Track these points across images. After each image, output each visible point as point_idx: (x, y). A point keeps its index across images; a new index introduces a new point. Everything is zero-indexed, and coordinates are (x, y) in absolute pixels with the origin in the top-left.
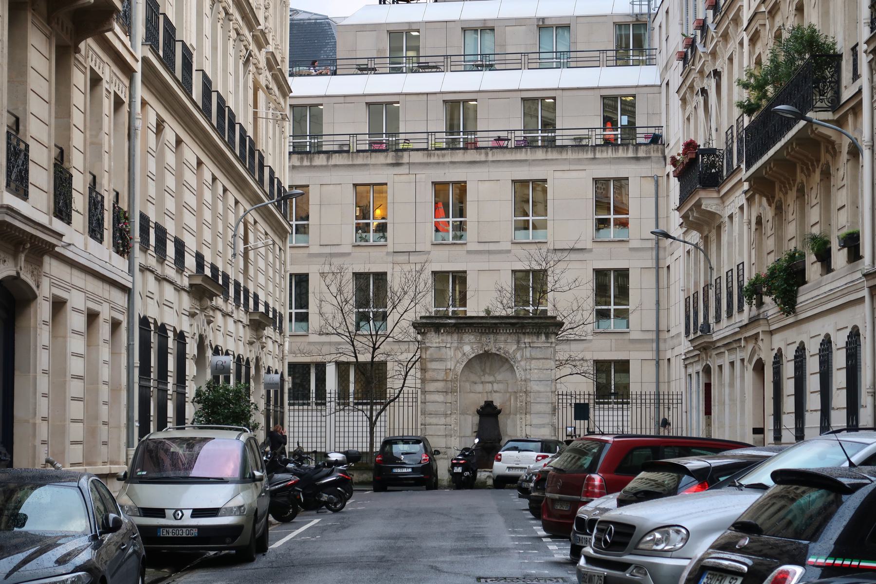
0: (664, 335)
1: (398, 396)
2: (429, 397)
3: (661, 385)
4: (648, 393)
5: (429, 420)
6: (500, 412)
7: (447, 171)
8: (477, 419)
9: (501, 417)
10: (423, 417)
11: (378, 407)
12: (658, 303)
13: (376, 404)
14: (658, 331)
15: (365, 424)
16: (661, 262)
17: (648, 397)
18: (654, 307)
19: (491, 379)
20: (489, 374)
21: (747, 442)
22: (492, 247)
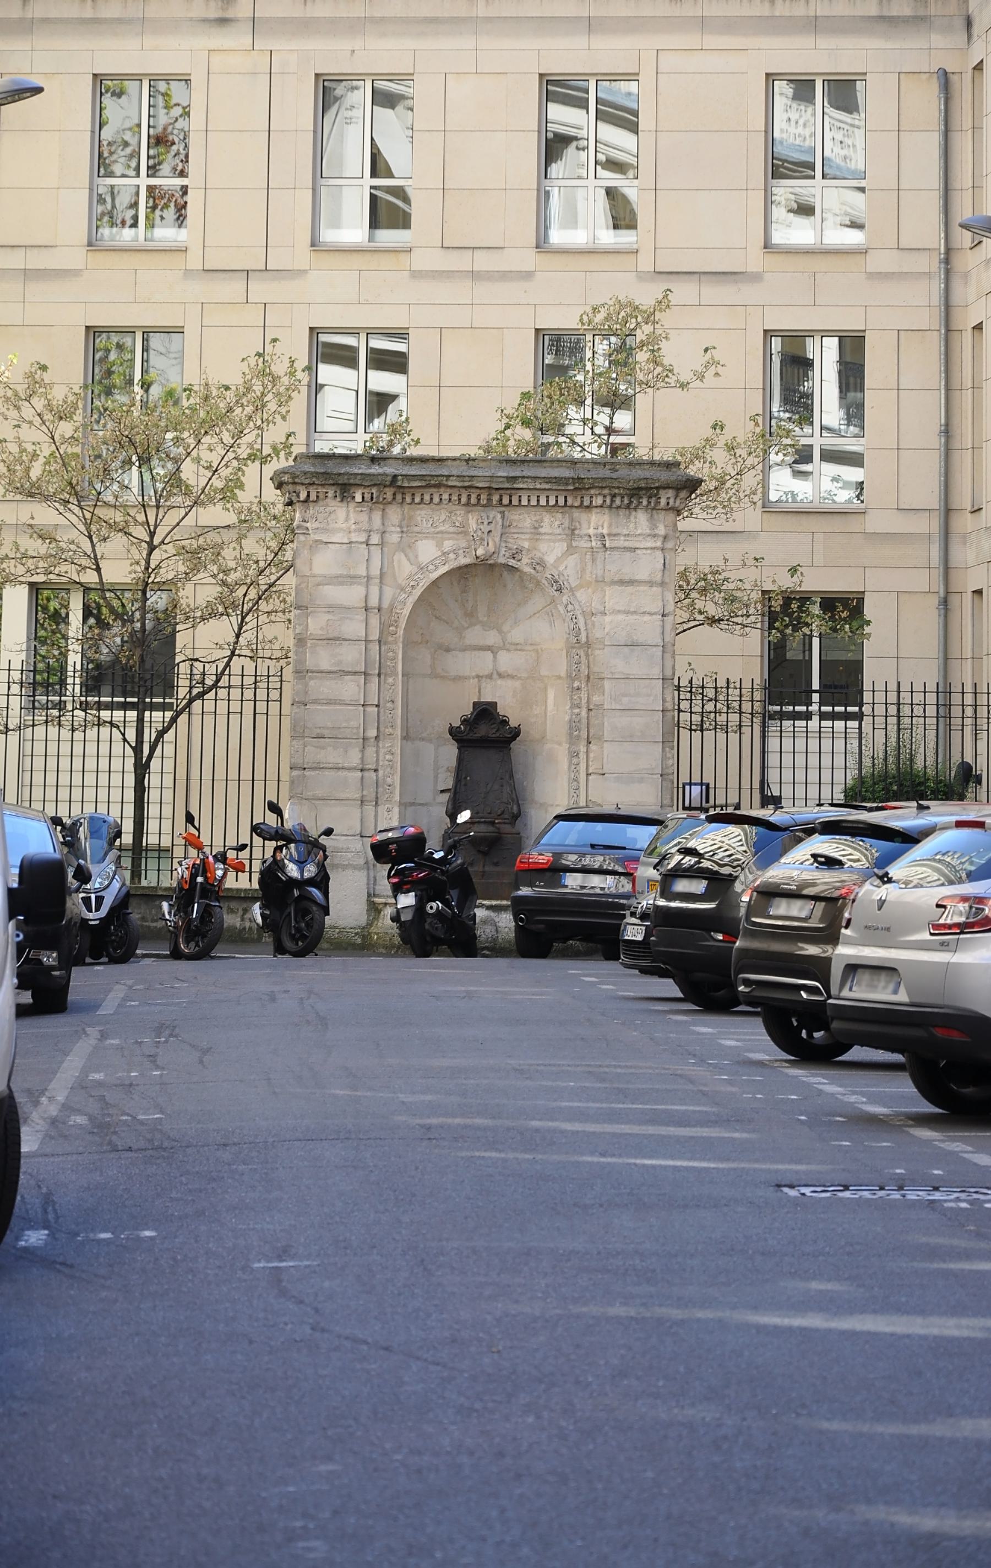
0: (964, 523)
1: (215, 686)
2: (322, 688)
3: (954, 664)
4: (918, 687)
5: (313, 754)
7: (358, 44)
8: (451, 751)
10: (297, 744)
11: (157, 715)
12: (947, 431)
13: (153, 707)
14: (948, 512)
15: (117, 764)
16: (956, 314)
17: (880, 697)
18: (936, 441)
19: (492, 638)
22: (483, 262)
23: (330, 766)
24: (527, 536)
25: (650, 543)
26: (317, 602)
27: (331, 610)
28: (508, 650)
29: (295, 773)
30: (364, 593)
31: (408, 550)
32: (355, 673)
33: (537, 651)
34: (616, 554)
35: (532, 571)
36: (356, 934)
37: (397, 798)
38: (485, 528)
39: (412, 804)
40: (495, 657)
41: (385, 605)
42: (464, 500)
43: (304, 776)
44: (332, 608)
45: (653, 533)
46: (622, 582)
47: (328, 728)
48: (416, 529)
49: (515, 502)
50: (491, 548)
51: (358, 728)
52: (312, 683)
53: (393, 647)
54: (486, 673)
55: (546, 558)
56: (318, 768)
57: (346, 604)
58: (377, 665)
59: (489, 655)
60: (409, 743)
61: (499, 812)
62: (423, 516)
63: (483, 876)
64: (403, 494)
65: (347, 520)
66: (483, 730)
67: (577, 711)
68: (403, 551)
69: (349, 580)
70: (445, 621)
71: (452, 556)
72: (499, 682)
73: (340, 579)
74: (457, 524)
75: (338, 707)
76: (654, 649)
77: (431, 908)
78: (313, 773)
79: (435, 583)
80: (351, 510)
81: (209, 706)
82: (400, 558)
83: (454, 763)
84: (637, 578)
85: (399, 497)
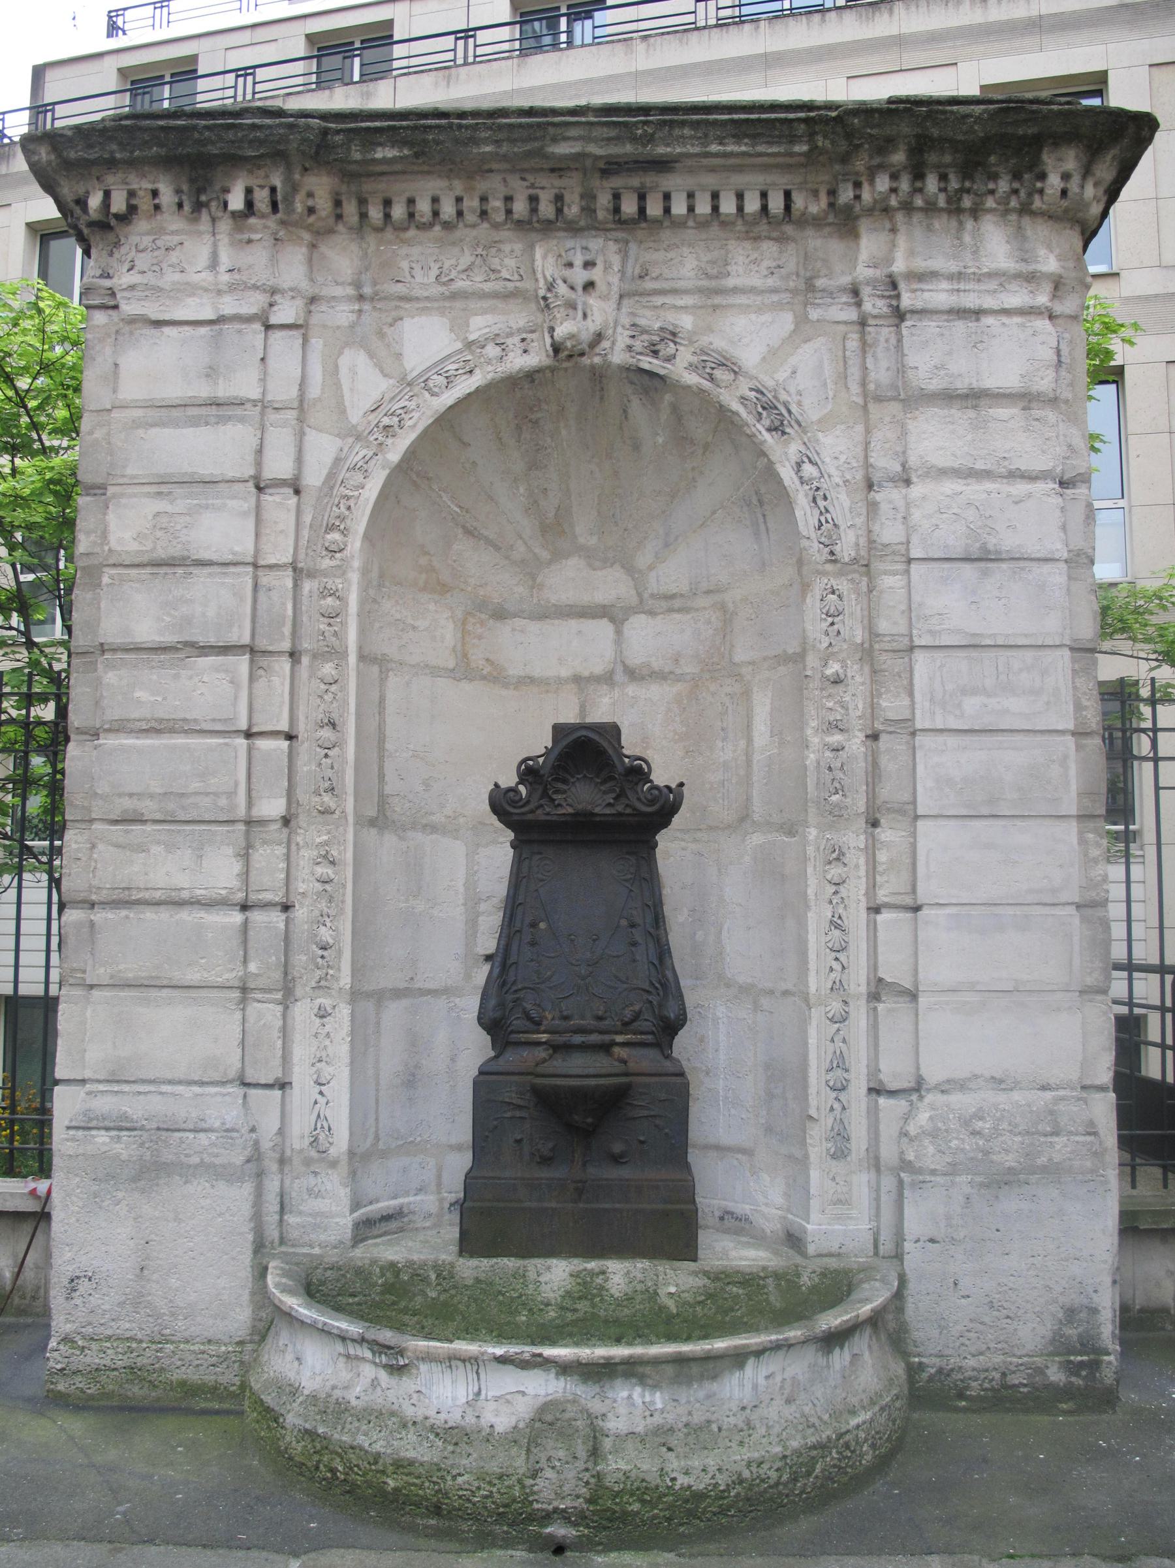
6: (665, 807)
8: (498, 854)
9: (671, 847)
19: (610, 586)
20: (596, 558)
21: (246, 1209)
23: (158, 895)
24: (688, 300)
25: (1016, 298)
26: (129, 471)
27: (164, 489)
28: (652, 613)
30: (255, 442)
32: (225, 650)
34: (930, 326)
35: (706, 384)
36: (225, 1357)
37: (345, 980)
38: (580, 276)
39: (398, 994)
40: (619, 632)
41: (313, 478)
43: (92, 924)
44: (165, 484)
45: (1024, 268)
46: (948, 397)
47: (151, 796)
48: (399, 289)
49: (654, 209)
51: (232, 794)
52: (110, 677)
53: (338, 583)
54: (598, 669)
56: (124, 901)
57: (206, 470)
58: (287, 630)
60: (390, 839)
61: (628, 1014)
62: (420, 262)
63: (580, 1192)
65: (214, 264)
66: (584, 796)
67: (836, 738)
68: (363, 344)
69: (213, 410)
70: (489, 542)
71: (492, 351)
72: (631, 690)
73: (192, 411)
74: (505, 274)
75: (180, 740)
76: (1046, 568)
78: (110, 915)
79: (448, 420)
80: (224, 240)
82: (354, 361)
83: (501, 890)
84: (989, 383)
85: (350, 209)
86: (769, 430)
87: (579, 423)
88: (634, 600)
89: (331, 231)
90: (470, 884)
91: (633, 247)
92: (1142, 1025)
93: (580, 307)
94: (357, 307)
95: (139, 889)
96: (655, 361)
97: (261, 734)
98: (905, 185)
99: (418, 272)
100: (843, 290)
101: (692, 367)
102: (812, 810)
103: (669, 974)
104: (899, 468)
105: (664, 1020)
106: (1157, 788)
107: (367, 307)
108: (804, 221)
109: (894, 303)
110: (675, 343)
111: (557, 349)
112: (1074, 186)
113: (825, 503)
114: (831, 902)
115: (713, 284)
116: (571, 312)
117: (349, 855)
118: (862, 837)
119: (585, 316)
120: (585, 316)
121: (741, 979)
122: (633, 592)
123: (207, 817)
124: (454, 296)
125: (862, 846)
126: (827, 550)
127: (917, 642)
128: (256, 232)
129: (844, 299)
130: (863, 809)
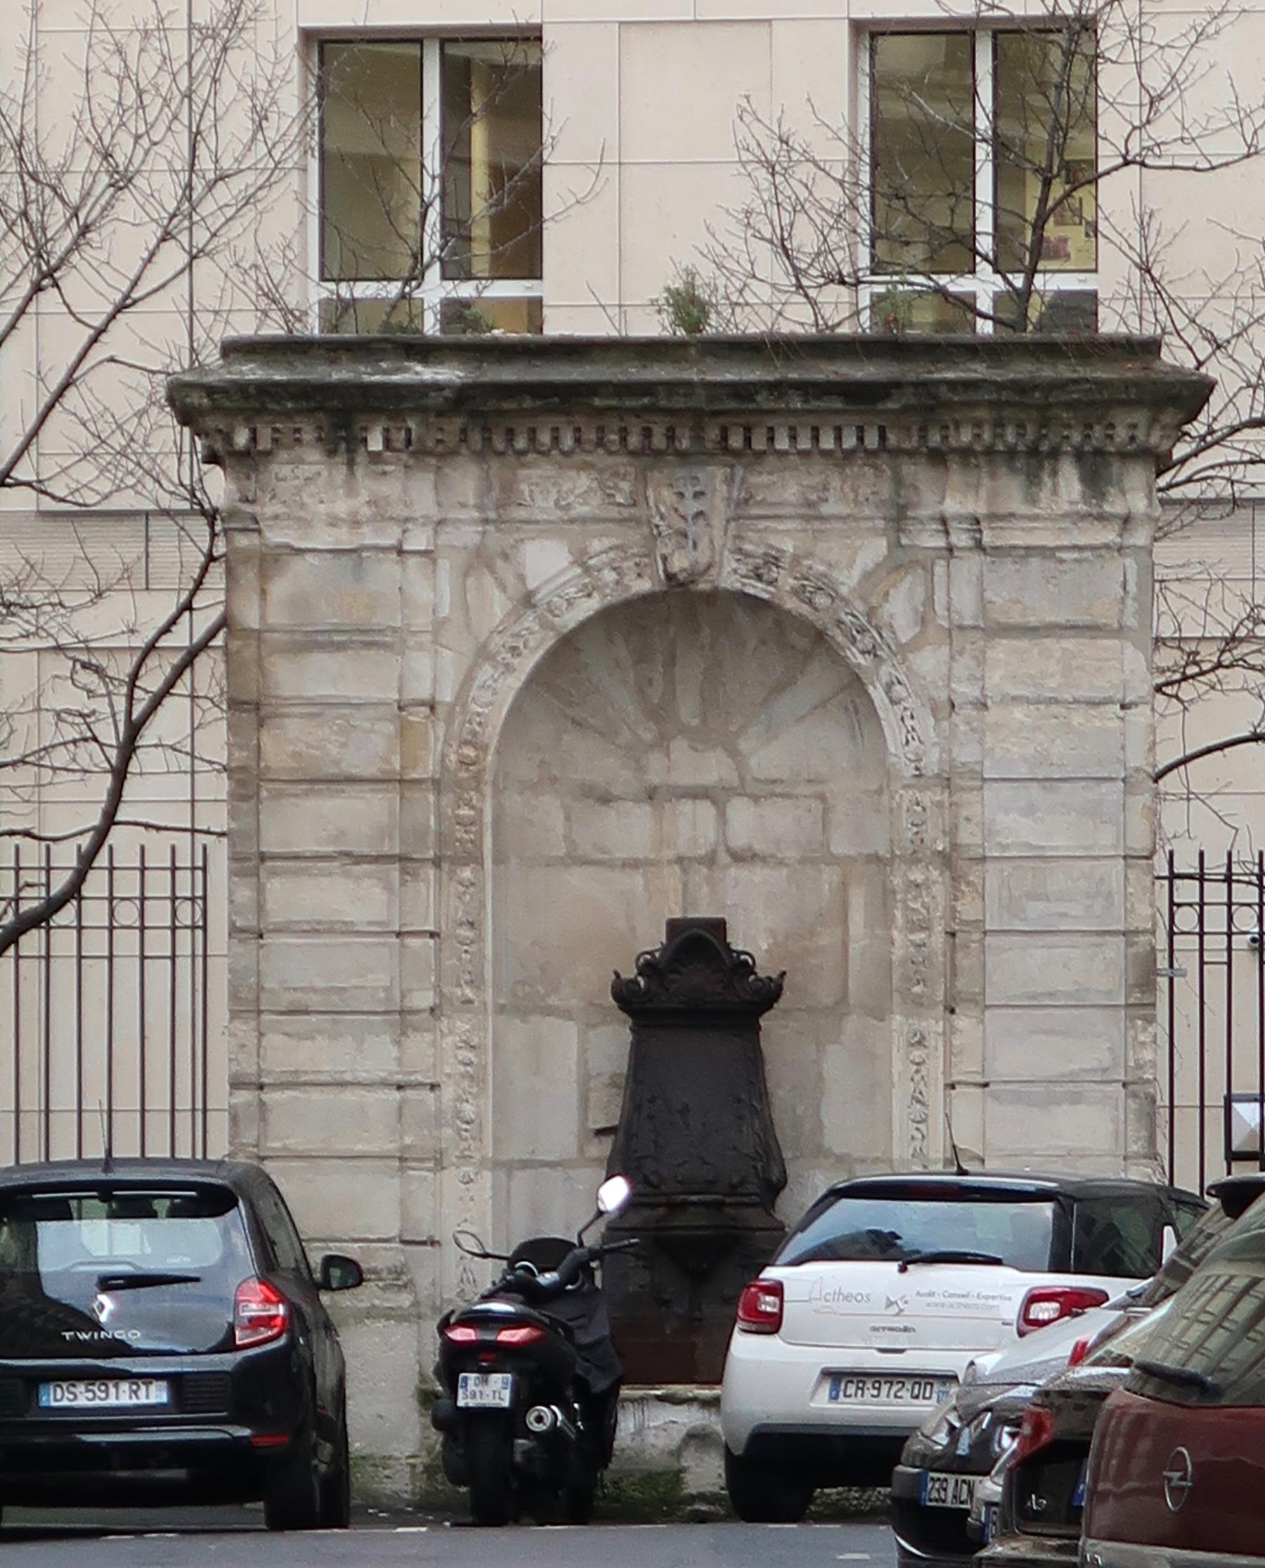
2: (289, 897)
5: (285, 1052)
8: (614, 1041)
10: (245, 1029)
19: (713, 768)
20: (701, 739)
29: (244, 1096)
31: (499, 563)
33: (822, 798)
38: (692, 507)
39: (525, 1164)
42: (634, 441)
43: (262, 1103)
44: (319, 708)
48: (522, 513)
50: (703, 556)
54: (701, 852)
55: (836, 575)
59: (706, 810)
64: (485, 429)
67: (919, 937)
68: (491, 569)
74: (620, 499)
76: (1104, 787)
77: (540, 1419)
81: (64, 942)
83: (621, 1064)
86: (863, 653)
87: (674, 632)
88: (736, 783)
89: (454, 453)
90: (583, 1062)
91: (739, 471)
92: (1117, 1193)
93: (690, 537)
94: (480, 529)
95: (306, 1073)
96: (759, 585)
97: (193, 806)
98: (987, 436)
99: (538, 497)
100: (933, 519)
101: (795, 592)
102: (896, 996)
103: (772, 1143)
104: (977, 693)
105: (768, 1182)
106: (1171, 934)
107: (491, 528)
108: (897, 453)
109: (978, 535)
110: (778, 567)
111: (670, 577)
112: (1140, 435)
113: (912, 723)
114: (912, 1079)
115: (811, 512)
116: (683, 541)
117: (490, 1043)
118: (941, 1023)
119: (695, 545)
120: (695, 545)
121: (837, 1151)
122: (736, 773)
123: (365, 1009)
124: (572, 521)
125: (940, 1030)
126: (913, 765)
127: (988, 854)
128: (391, 464)
129: (934, 527)
130: (942, 998)
